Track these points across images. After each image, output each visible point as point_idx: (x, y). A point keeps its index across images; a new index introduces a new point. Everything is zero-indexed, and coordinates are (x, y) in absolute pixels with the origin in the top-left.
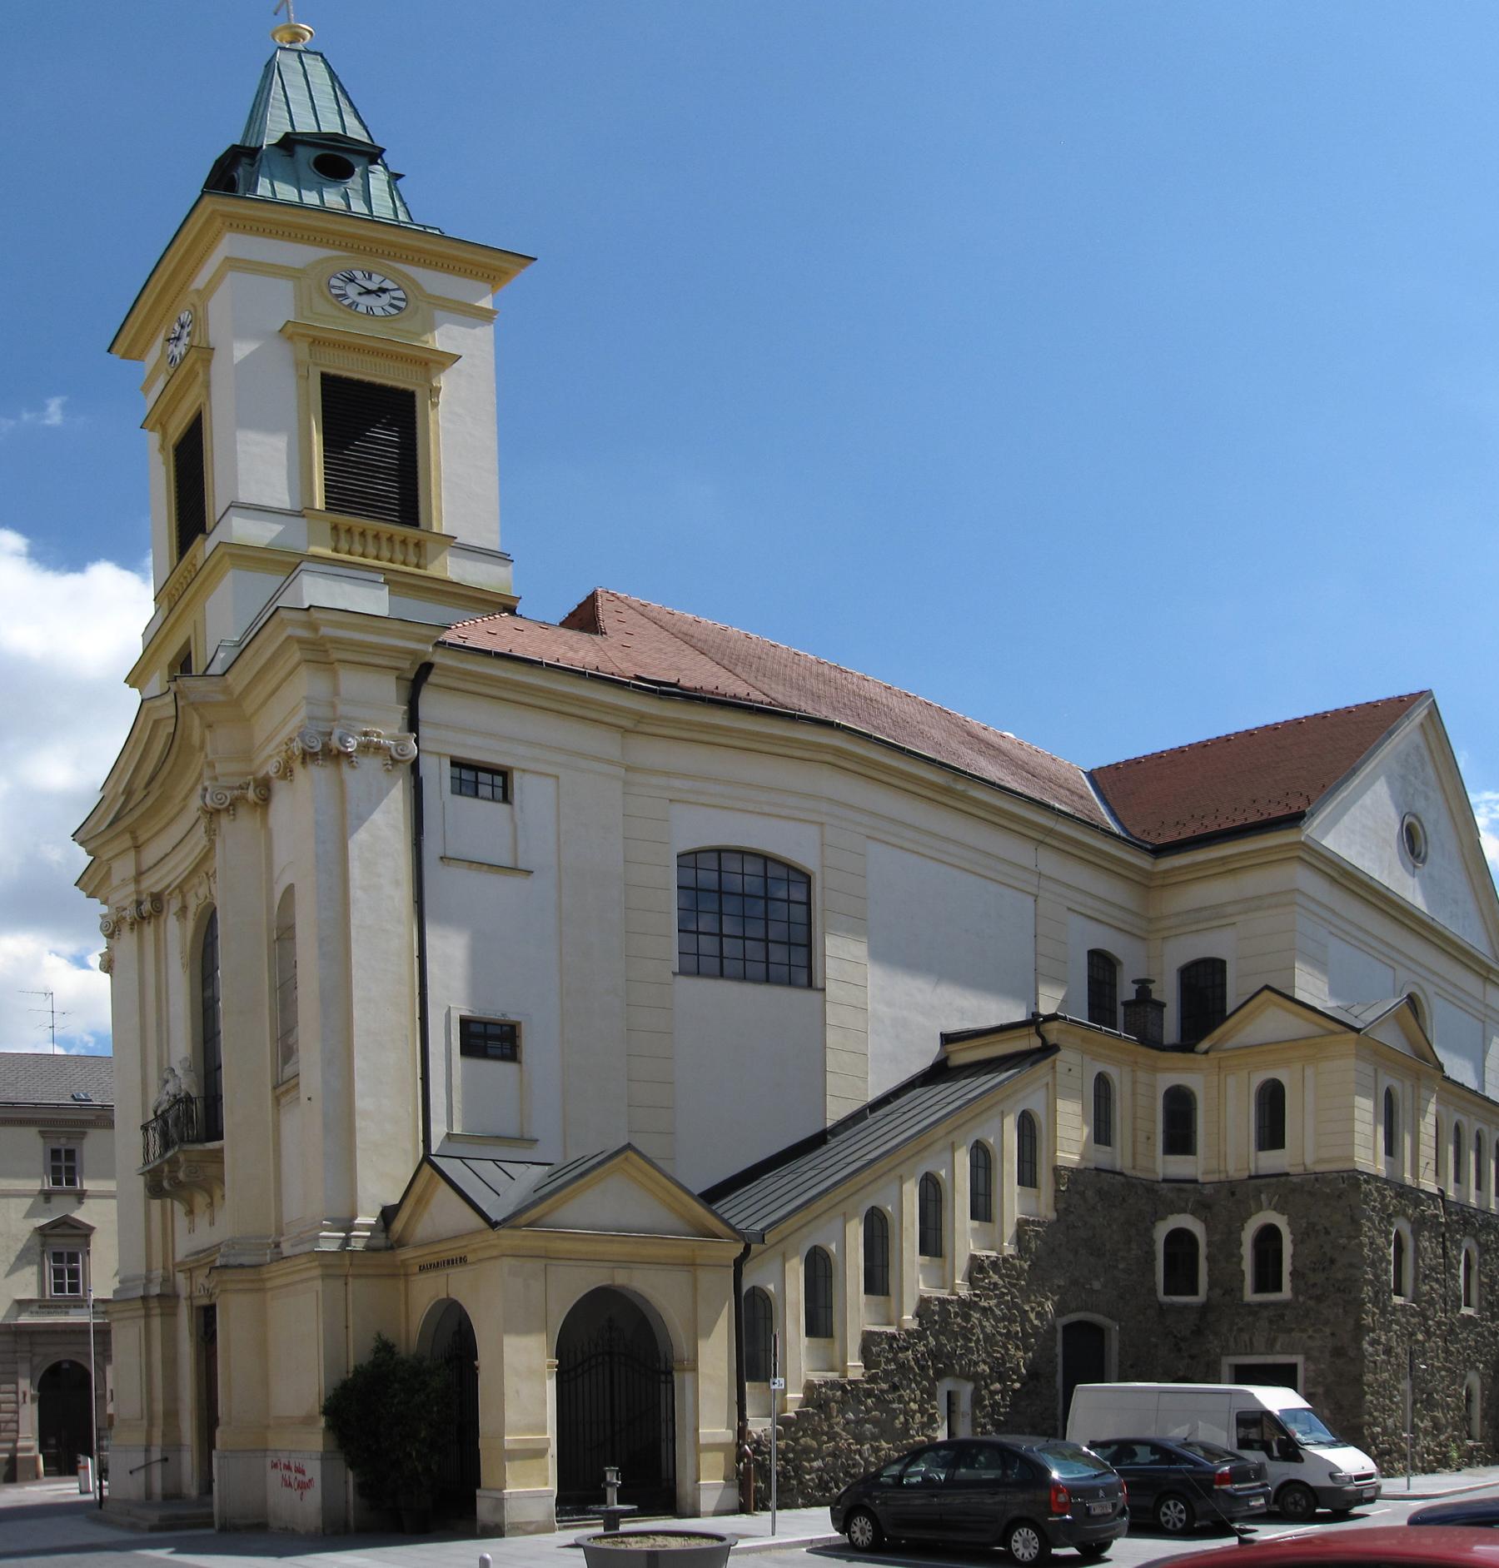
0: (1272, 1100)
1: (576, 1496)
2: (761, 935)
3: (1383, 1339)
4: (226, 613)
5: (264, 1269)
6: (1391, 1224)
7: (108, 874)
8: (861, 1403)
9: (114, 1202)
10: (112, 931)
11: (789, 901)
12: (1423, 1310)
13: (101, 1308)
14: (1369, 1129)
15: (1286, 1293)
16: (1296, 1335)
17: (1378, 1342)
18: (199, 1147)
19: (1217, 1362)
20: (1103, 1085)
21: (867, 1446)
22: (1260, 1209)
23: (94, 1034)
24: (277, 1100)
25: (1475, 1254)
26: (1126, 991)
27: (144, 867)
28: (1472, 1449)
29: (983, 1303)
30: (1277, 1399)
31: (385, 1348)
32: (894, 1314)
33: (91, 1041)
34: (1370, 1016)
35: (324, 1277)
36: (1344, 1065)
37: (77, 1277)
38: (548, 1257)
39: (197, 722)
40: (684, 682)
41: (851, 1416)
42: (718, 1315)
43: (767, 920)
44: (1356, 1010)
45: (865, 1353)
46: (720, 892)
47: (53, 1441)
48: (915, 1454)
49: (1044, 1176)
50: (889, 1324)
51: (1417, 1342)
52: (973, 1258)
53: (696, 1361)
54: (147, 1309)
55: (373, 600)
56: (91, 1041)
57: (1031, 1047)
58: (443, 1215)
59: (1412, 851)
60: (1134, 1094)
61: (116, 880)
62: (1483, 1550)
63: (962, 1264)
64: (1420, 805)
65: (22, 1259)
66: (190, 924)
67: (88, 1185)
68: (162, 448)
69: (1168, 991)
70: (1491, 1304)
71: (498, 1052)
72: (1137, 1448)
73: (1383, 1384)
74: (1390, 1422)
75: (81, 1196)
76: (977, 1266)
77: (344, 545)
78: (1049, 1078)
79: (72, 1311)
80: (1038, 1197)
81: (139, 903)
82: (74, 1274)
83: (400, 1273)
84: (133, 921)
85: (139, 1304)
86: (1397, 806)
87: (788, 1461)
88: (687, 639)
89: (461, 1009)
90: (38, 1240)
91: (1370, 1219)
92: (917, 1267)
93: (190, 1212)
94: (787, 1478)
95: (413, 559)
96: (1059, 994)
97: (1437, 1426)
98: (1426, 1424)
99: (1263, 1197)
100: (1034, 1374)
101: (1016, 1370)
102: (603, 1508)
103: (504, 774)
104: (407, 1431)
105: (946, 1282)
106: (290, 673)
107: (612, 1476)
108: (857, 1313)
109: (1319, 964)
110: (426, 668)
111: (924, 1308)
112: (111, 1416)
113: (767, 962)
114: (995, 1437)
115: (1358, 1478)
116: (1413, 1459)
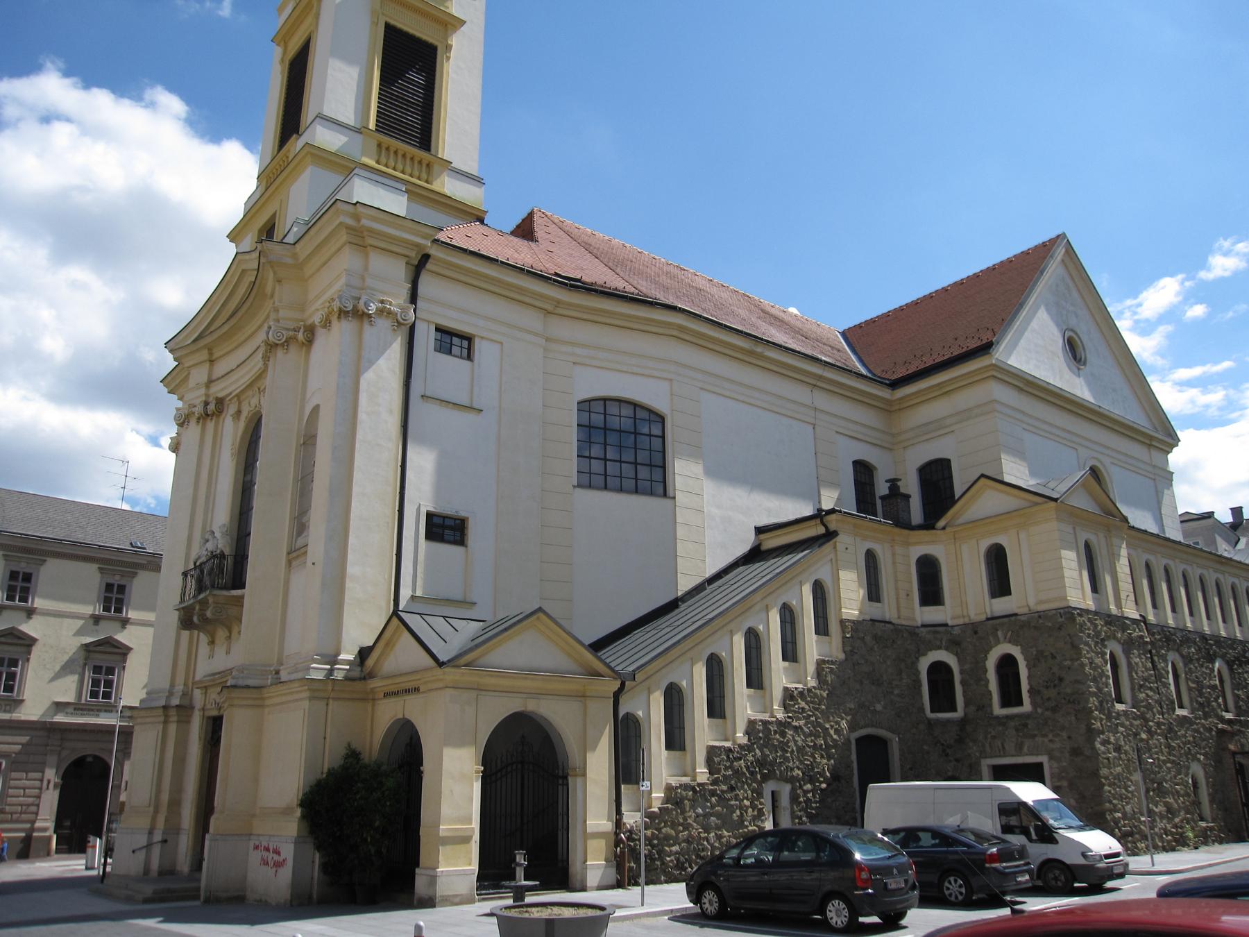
0: (997, 560)
1: (492, 875)
2: (632, 460)
3: (1112, 739)
4: (302, 199)
5: (265, 690)
6: (1105, 647)
7: (186, 378)
8: (707, 800)
9: (151, 630)
10: (183, 421)
11: (650, 435)
12: (1143, 713)
13: (128, 713)
14: (1076, 574)
15: (1027, 707)
16: (1039, 739)
17: (1109, 743)
18: (225, 593)
19: (979, 764)
20: (871, 557)
21: (712, 834)
22: (998, 642)
23: (156, 498)
24: (289, 563)
25: (1180, 665)
26: (882, 489)
27: (214, 377)
28: (1206, 829)
29: (795, 723)
30: (1030, 792)
31: (353, 755)
32: (729, 733)
33: (153, 503)
34: (1063, 488)
35: (311, 698)
36: (1048, 527)
37: (111, 687)
38: (479, 689)
39: (271, 275)
40: (584, 279)
41: (700, 810)
42: (602, 734)
43: (636, 449)
44: (1052, 485)
45: (710, 762)
46: (605, 429)
47: (68, 823)
48: (749, 840)
49: (834, 627)
50: (726, 740)
51: (1142, 740)
52: (786, 689)
53: (585, 768)
54: (166, 716)
55: (396, 203)
56: (153, 503)
57: (818, 534)
58: (405, 655)
59: (1075, 358)
60: (894, 563)
61: (192, 383)
62: (1230, 920)
63: (778, 694)
64: (1073, 322)
65: (66, 669)
66: (242, 424)
67: (132, 614)
68: (282, 60)
69: (911, 486)
70: (1201, 704)
71: (452, 538)
72: (921, 834)
73: (1118, 777)
74: (1128, 808)
75: (125, 622)
76: (789, 695)
77: (383, 160)
78: (832, 556)
79: (102, 714)
80: (830, 643)
81: (206, 404)
82: (109, 684)
83: (369, 698)
84: (200, 416)
85: (161, 712)
86: (1058, 325)
87: (653, 846)
88: (587, 247)
89: (428, 506)
90: (82, 654)
91: (1087, 644)
92: (745, 697)
93: (212, 642)
94: (653, 860)
95: (424, 176)
96: (835, 494)
97: (1169, 809)
98: (1160, 809)
99: (1000, 633)
100: (836, 777)
101: (822, 774)
102: (513, 884)
103: (469, 339)
104: (363, 830)
105: (767, 708)
106: (339, 250)
107: (521, 858)
108: (703, 733)
109: (1019, 454)
110: (426, 257)
111: (751, 728)
112: (123, 804)
113: (636, 479)
114: (809, 827)
115: (1108, 856)
116: (1153, 839)
